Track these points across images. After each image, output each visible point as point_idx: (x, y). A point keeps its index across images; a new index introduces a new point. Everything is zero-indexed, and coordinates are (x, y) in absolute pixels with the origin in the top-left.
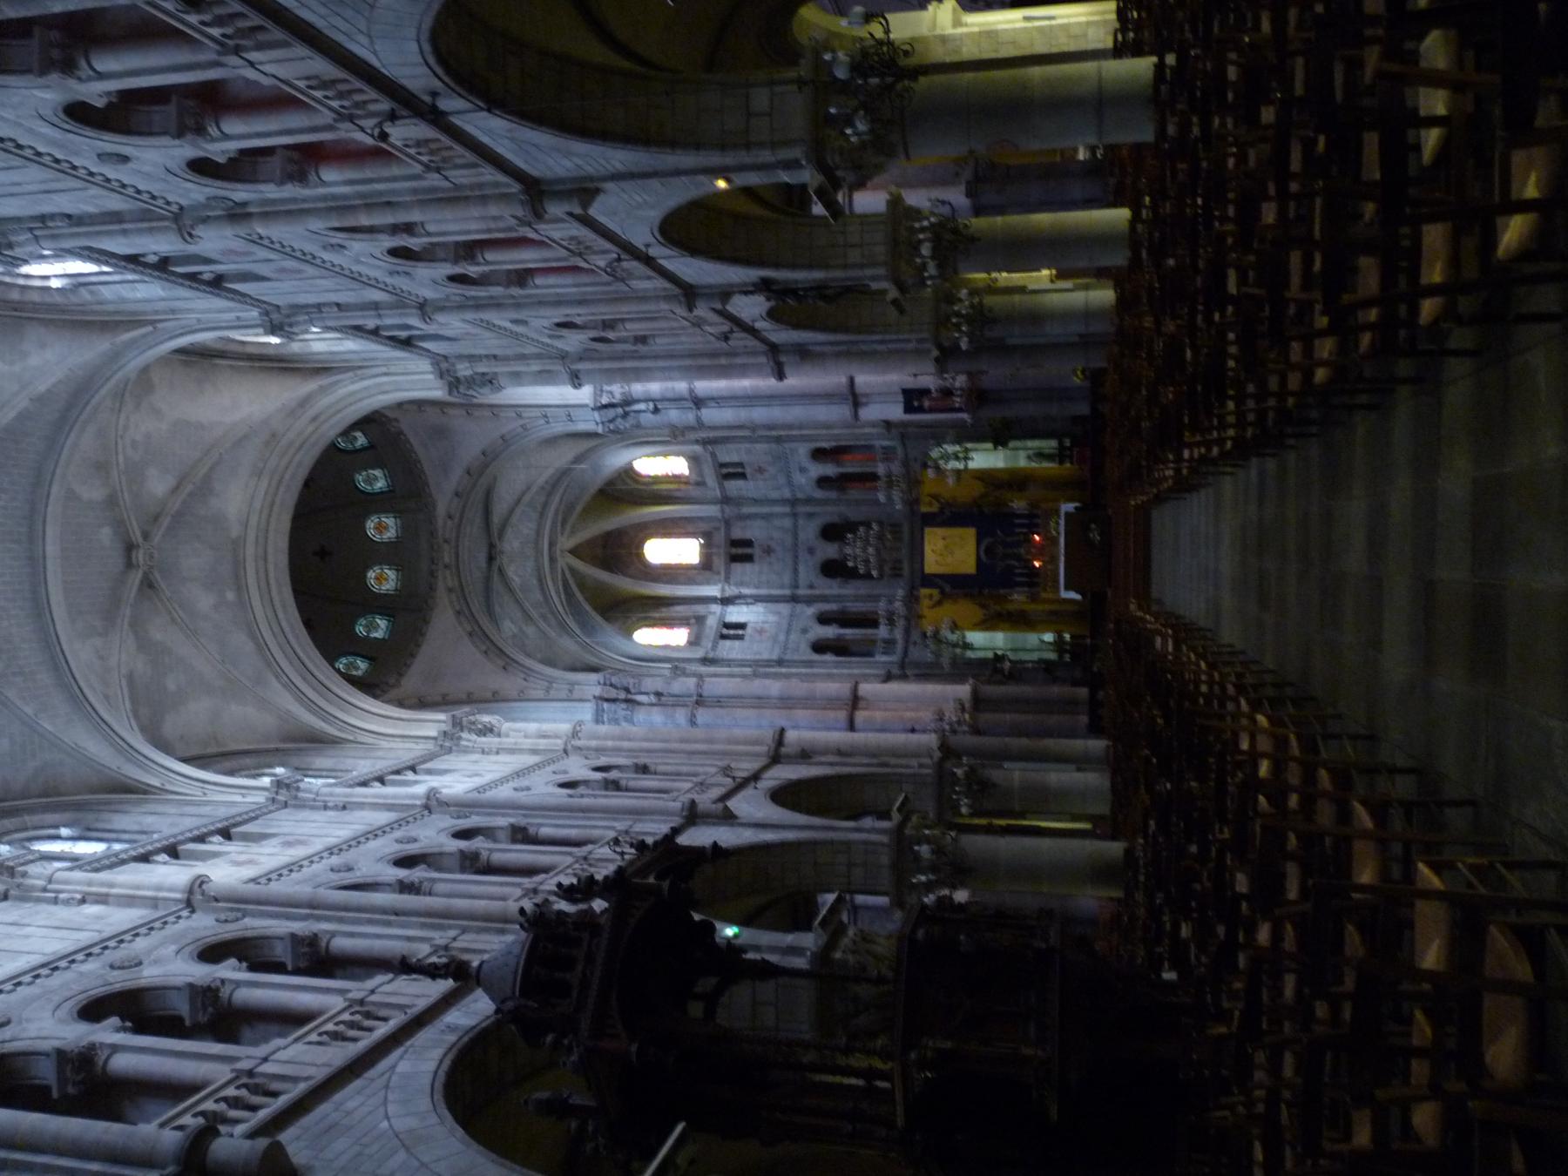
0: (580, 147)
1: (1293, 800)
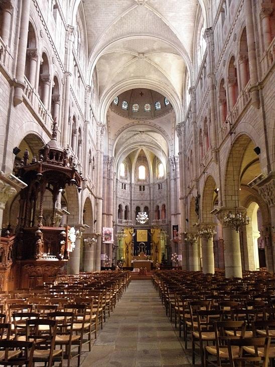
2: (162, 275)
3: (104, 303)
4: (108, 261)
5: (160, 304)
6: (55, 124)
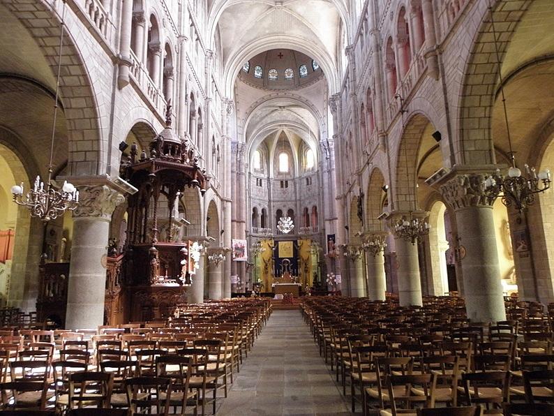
0: (396, 148)
1: (201, 368)
2: (314, 302)
3: (239, 340)
4: (241, 285)
5: (312, 342)
6: (169, 107)
